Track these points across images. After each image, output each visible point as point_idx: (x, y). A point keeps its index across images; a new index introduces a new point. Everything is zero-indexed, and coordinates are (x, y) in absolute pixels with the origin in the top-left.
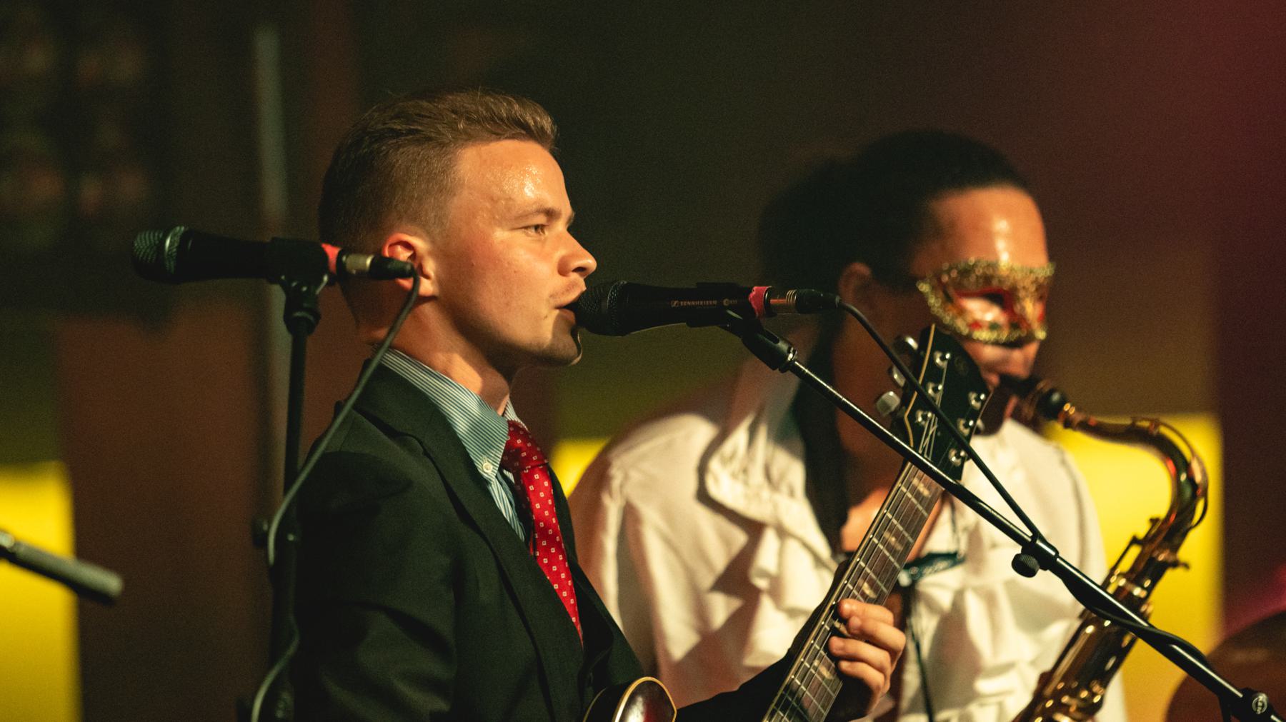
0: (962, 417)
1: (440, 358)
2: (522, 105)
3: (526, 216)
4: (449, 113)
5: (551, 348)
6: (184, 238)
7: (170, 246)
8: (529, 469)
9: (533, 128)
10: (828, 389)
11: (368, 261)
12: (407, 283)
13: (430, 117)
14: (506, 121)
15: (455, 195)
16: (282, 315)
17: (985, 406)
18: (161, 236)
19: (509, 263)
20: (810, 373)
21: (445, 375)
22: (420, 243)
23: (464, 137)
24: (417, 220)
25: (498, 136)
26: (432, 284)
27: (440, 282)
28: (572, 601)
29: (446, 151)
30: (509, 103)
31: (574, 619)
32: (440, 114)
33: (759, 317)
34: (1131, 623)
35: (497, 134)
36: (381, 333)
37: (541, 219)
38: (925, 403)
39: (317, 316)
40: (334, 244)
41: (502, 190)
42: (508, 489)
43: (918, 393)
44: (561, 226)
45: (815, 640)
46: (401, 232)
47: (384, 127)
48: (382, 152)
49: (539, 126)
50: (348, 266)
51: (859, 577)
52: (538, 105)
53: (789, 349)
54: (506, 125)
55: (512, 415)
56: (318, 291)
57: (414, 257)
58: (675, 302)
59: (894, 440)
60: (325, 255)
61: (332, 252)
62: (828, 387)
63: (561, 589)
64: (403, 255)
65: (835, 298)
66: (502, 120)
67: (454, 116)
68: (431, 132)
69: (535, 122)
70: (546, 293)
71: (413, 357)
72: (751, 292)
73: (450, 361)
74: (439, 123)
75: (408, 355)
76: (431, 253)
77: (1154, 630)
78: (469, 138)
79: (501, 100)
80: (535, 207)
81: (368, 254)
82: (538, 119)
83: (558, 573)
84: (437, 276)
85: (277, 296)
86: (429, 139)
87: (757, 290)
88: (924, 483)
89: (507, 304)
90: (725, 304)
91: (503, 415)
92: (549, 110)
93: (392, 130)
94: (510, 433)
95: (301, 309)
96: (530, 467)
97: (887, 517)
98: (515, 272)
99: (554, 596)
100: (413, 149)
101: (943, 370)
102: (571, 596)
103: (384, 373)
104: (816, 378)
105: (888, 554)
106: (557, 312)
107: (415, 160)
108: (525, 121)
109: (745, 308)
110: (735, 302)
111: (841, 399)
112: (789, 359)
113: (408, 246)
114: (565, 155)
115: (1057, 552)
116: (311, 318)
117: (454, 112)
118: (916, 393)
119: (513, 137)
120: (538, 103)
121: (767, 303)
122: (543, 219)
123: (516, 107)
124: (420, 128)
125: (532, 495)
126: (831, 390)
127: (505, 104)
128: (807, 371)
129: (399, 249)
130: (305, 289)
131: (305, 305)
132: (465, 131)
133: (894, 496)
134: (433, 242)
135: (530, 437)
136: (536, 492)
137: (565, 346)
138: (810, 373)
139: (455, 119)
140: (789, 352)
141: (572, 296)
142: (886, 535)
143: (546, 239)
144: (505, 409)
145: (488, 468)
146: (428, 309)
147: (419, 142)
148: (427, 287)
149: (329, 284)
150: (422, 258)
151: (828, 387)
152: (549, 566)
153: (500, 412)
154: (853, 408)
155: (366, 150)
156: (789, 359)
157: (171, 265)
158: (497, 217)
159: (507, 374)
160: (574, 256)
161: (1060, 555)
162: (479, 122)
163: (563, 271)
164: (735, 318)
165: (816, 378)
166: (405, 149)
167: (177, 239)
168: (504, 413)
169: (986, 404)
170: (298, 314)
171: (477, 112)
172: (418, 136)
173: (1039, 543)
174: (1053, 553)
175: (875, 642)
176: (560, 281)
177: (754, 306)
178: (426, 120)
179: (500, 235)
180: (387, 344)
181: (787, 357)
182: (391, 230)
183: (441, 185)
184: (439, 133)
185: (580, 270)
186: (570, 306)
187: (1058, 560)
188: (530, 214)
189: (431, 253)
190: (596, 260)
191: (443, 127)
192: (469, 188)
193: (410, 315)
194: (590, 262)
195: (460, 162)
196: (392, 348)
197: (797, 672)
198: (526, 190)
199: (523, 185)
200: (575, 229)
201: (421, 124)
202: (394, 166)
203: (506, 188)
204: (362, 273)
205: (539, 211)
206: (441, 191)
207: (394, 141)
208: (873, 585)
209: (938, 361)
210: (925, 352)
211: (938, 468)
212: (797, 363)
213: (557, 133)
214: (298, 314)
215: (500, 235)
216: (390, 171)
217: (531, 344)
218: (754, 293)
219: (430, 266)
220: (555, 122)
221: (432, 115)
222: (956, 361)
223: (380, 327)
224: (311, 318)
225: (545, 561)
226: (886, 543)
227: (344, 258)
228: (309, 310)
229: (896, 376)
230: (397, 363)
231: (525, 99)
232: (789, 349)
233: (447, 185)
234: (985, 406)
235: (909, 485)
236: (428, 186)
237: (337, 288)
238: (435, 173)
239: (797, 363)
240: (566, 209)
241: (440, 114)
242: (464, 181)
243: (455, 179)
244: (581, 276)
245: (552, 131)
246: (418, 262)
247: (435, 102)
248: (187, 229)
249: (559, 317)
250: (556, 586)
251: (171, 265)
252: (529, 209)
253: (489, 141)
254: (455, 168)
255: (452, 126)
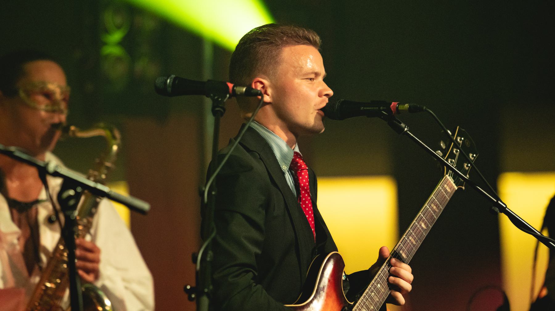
0: (466, 163)
1: (271, 127)
2: (309, 32)
3: (308, 74)
4: (280, 33)
5: (314, 126)
6: (175, 79)
7: (169, 82)
8: (300, 170)
9: (312, 41)
10: (420, 142)
11: (244, 89)
12: (260, 97)
13: (273, 34)
14: (302, 37)
15: (280, 65)
16: (211, 109)
17: (475, 159)
18: (166, 78)
19: (300, 92)
20: (413, 136)
21: (273, 132)
22: (266, 82)
23: (286, 43)
24: (266, 74)
25: (298, 43)
26: (270, 98)
27: (273, 97)
28: (313, 222)
29: (278, 48)
30: (304, 31)
31: (313, 230)
32: (277, 34)
33: (394, 114)
34: (535, 234)
35: (298, 42)
36: (250, 115)
37: (313, 76)
38: (452, 156)
39: (224, 110)
40: (231, 83)
41: (299, 64)
42: (292, 177)
43: (454, 143)
44: (320, 79)
45: (416, 221)
46: (259, 77)
47: (255, 37)
48: (254, 47)
49: (314, 40)
50: (237, 91)
51: (420, 221)
52: (315, 32)
53: (405, 126)
54: (302, 39)
55: (297, 150)
56: (225, 100)
57: (263, 87)
58: (362, 108)
59: (445, 162)
60: (228, 87)
61: (231, 86)
62: (420, 141)
63: (309, 218)
64: (259, 87)
65: (423, 107)
66: (300, 37)
67: (282, 34)
68: (273, 40)
69: (313, 37)
70: (313, 104)
71: (260, 123)
72: (391, 104)
73: (275, 128)
74: (276, 37)
75: (258, 122)
76: (270, 86)
77: (543, 236)
78: (287, 43)
79: (300, 29)
80: (311, 71)
81: (244, 86)
82: (314, 37)
83: (308, 211)
84: (272, 95)
85: (208, 102)
86: (272, 43)
87: (393, 104)
88: (449, 187)
89: (298, 107)
90: (381, 109)
91: (293, 150)
92: (319, 34)
93: (259, 39)
94: (294, 156)
95: (219, 107)
96: (300, 169)
97: (440, 189)
98: (302, 95)
99: (306, 220)
100: (265, 46)
101: (460, 144)
102: (312, 220)
103: (251, 129)
104: (415, 137)
105: (438, 203)
106: (317, 111)
107: (266, 51)
108: (309, 37)
109: (389, 110)
110: (385, 108)
111: (425, 146)
112: (405, 130)
113: (261, 83)
114: (323, 52)
115: (506, 206)
116: (222, 110)
117: (282, 33)
118: (453, 143)
119: (304, 44)
120: (315, 31)
121: (397, 108)
122: (312, 77)
123: (306, 32)
124: (269, 38)
125: (300, 181)
126: (421, 142)
127: (302, 31)
128: (412, 135)
129: (258, 84)
130: (220, 99)
131: (220, 106)
132: (286, 41)
133: (424, 209)
134: (271, 82)
135: (302, 158)
136: (302, 179)
137: (318, 125)
138: (413, 136)
139: (282, 35)
140: (405, 128)
141: (324, 105)
142: (432, 205)
143: (314, 83)
144: (295, 147)
145: (285, 168)
146: (268, 108)
147: (269, 44)
148: (267, 99)
149: (229, 98)
150: (267, 88)
151: (420, 141)
152: (305, 208)
153: (293, 149)
154: (429, 149)
155: (248, 46)
156: (405, 130)
157: (169, 89)
158: (296, 74)
159: (296, 135)
160: (325, 90)
161: (507, 207)
162: (291, 37)
163: (320, 95)
164: (385, 114)
165: (415, 137)
166: (263, 46)
167: (172, 80)
168: (294, 149)
169: (476, 158)
170: (217, 109)
171: (291, 33)
172: (268, 42)
173: (499, 202)
174: (505, 206)
175: (403, 278)
176: (319, 99)
177: (392, 110)
178: (271, 36)
179: (297, 81)
180: (252, 119)
181: (404, 129)
182: (255, 76)
183: (275, 61)
184: (276, 40)
185: (327, 95)
186: (322, 109)
187: (507, 209)
188: (309, 74)
189: (270, 86)
190: (333, 91)
191: (278, 39)
192: (286, 62)
193: (260, 109)
194: (331, 92)
195: (283, 52)
196: (253, 120)
197: (422, 212)
198: (308, 65)
199: (307, 62)
200: (325, 80)
201: (270, 37)
202: (258, 52)
203: (300, 63)
204: (242, 94)
205: (312, 73)
206: (275, 63)
207: (259, 43)
208: (425, 224)
209: (459, 140)
210: (454, 136)
211: (461, 173)
212: (408, 132)
213: (321, 43)
214: (217, 109)
215: (297, 81)
216: (257, 54)
217: (306, 123)
218: (392, 105)
219: (269, 91)
220: (321, 38)
221: (274, 34)
222: (465, 141)
223: (250, 112)
224: (222, 110)
225: (304, 206)
226: (432, 208)
227: (235, 88)
228: (221, 107)
229: (442, 145)
230: (255, 126)
231: (310, 30)
232: (405, 126)
233: (277, 61)
234: (475, 159)
235: (430, 206)
236: (270, 61)
237: (234, 99)
238: (273, 56)
239: (408, 132)
240: (323, 72)
241: (277, 34)
242: (284, 59)
243: (281, 58)
244: (327, 97)
245: (320, 42)
246: (265, 89)
247: (275, 29)
248: (176, 76)
249: (317, 113)
250: (307, 216)
251: (169, 89)
252: (309, 71)
253: (295, 45)
254: (281, 54)
255: (281, 39)
